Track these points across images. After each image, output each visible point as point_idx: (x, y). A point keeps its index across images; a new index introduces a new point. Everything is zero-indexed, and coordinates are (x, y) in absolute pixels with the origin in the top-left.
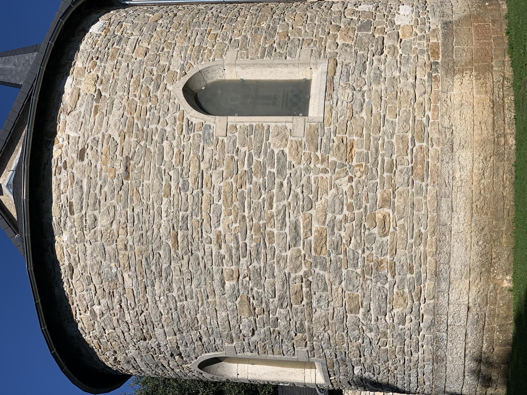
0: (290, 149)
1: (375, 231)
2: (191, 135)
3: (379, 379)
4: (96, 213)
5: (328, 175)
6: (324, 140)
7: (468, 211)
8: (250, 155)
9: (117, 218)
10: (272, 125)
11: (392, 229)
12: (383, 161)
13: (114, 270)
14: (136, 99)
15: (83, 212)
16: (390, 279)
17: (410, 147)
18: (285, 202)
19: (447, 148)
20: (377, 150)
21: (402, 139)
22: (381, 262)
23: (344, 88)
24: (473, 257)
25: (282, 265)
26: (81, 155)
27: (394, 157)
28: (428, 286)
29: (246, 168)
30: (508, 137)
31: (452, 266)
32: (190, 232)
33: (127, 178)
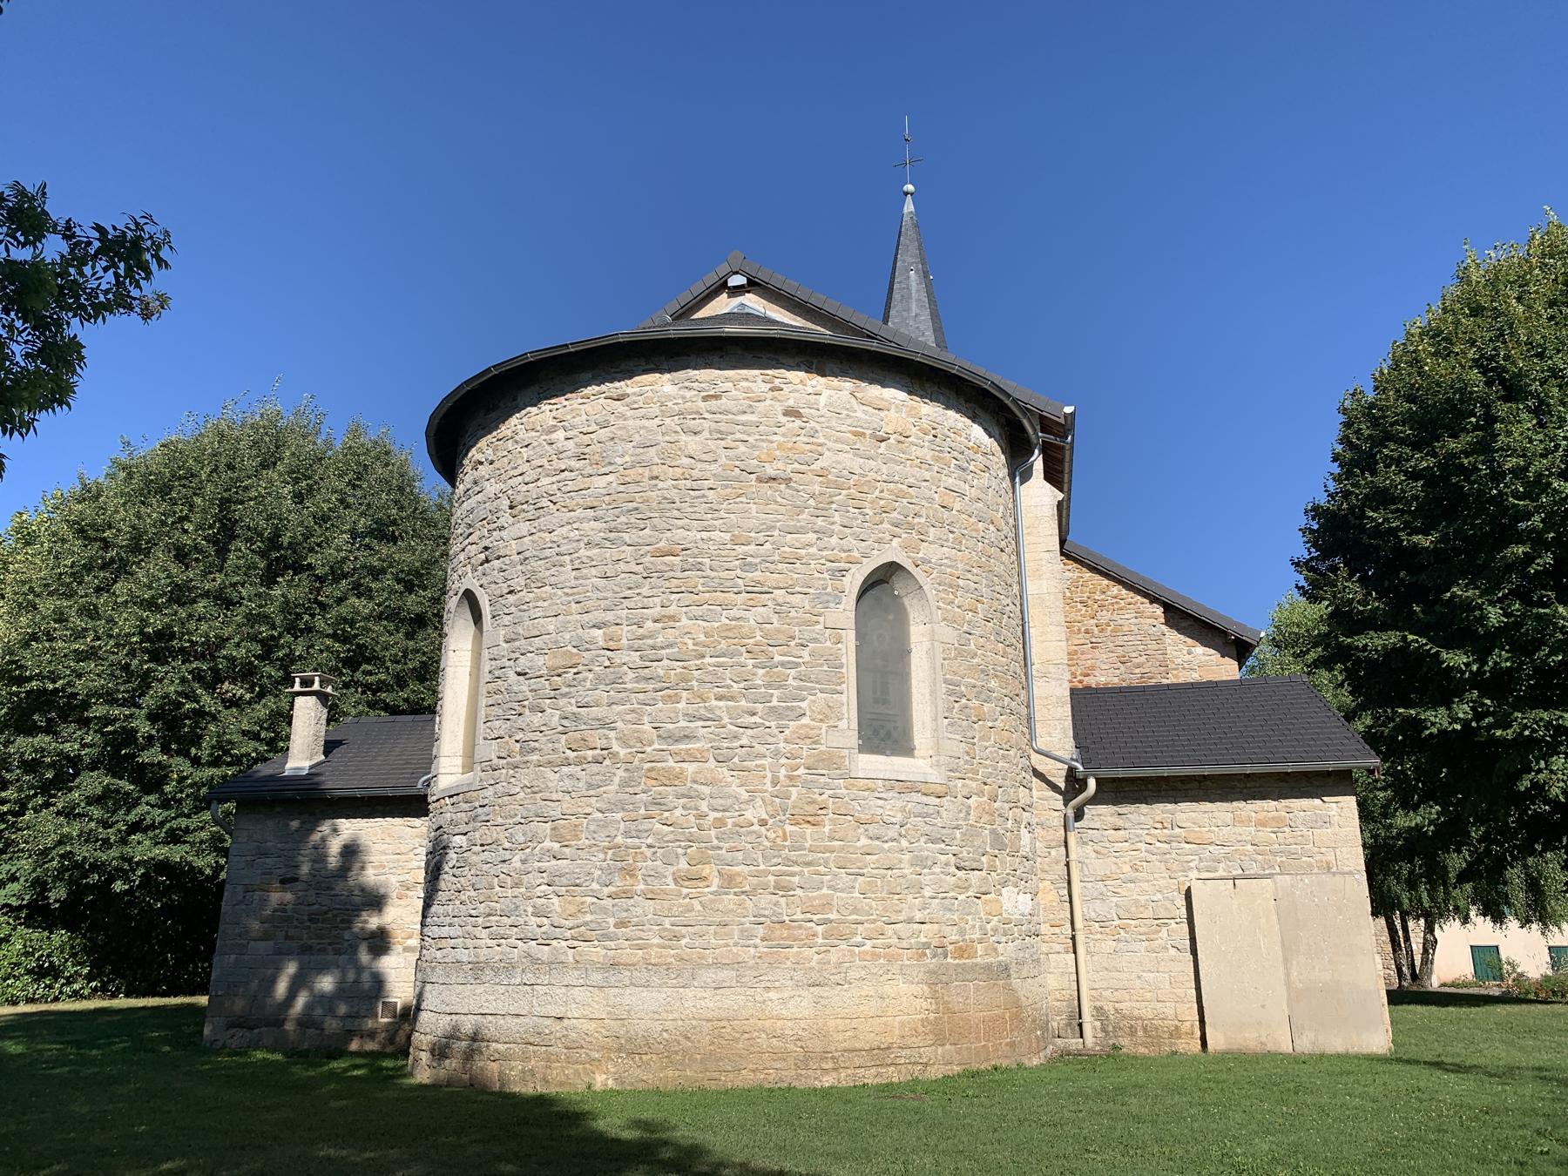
0: (807, 726)
1: (683, 865)
2: (826, 575)
4: (706, 434)
5: (769, 787)
6: (822, 779)
7: (715, 1014)
8: (797, 665)
9: (699, 465)
10: (844, 698)
11: (685, 891)
12: (792, 874)
13: (619, 461)
14: (877, 493)
15: (706, 415)
16: (606, 890)
17: (815, 918)
18: (726, 720)
19: (815, 977)
20: (809, 864)
21: (827, 905)
22: (632, 876)
23: (903, 810)
24: (643, 1024)
25: (628, 717)
26: (792, 413)
27: (799, 892)
28: (595, 952)
29: (778, 658)
30: (834, 1075)
31: (628, 991)
32: (678, 574)
33: (759, 480)
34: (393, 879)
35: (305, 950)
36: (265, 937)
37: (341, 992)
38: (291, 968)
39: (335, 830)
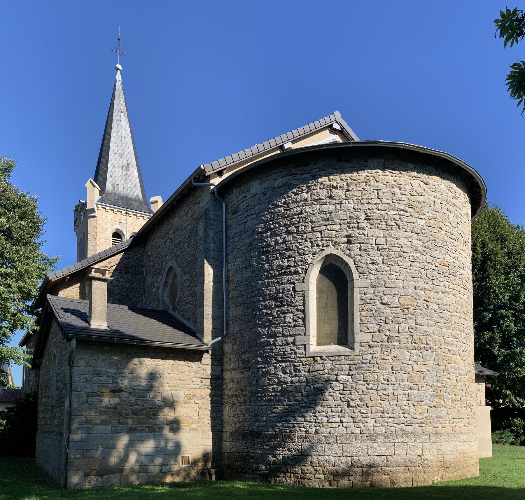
3: (225, 400)
13: (427, 215)
28: (429, 429)
31: (443, 444)
34: (182, 393)
35: (131, 430)
36: (104, 423)
37: (158, 451)
38: (124, 440)
39: (141, 363)
